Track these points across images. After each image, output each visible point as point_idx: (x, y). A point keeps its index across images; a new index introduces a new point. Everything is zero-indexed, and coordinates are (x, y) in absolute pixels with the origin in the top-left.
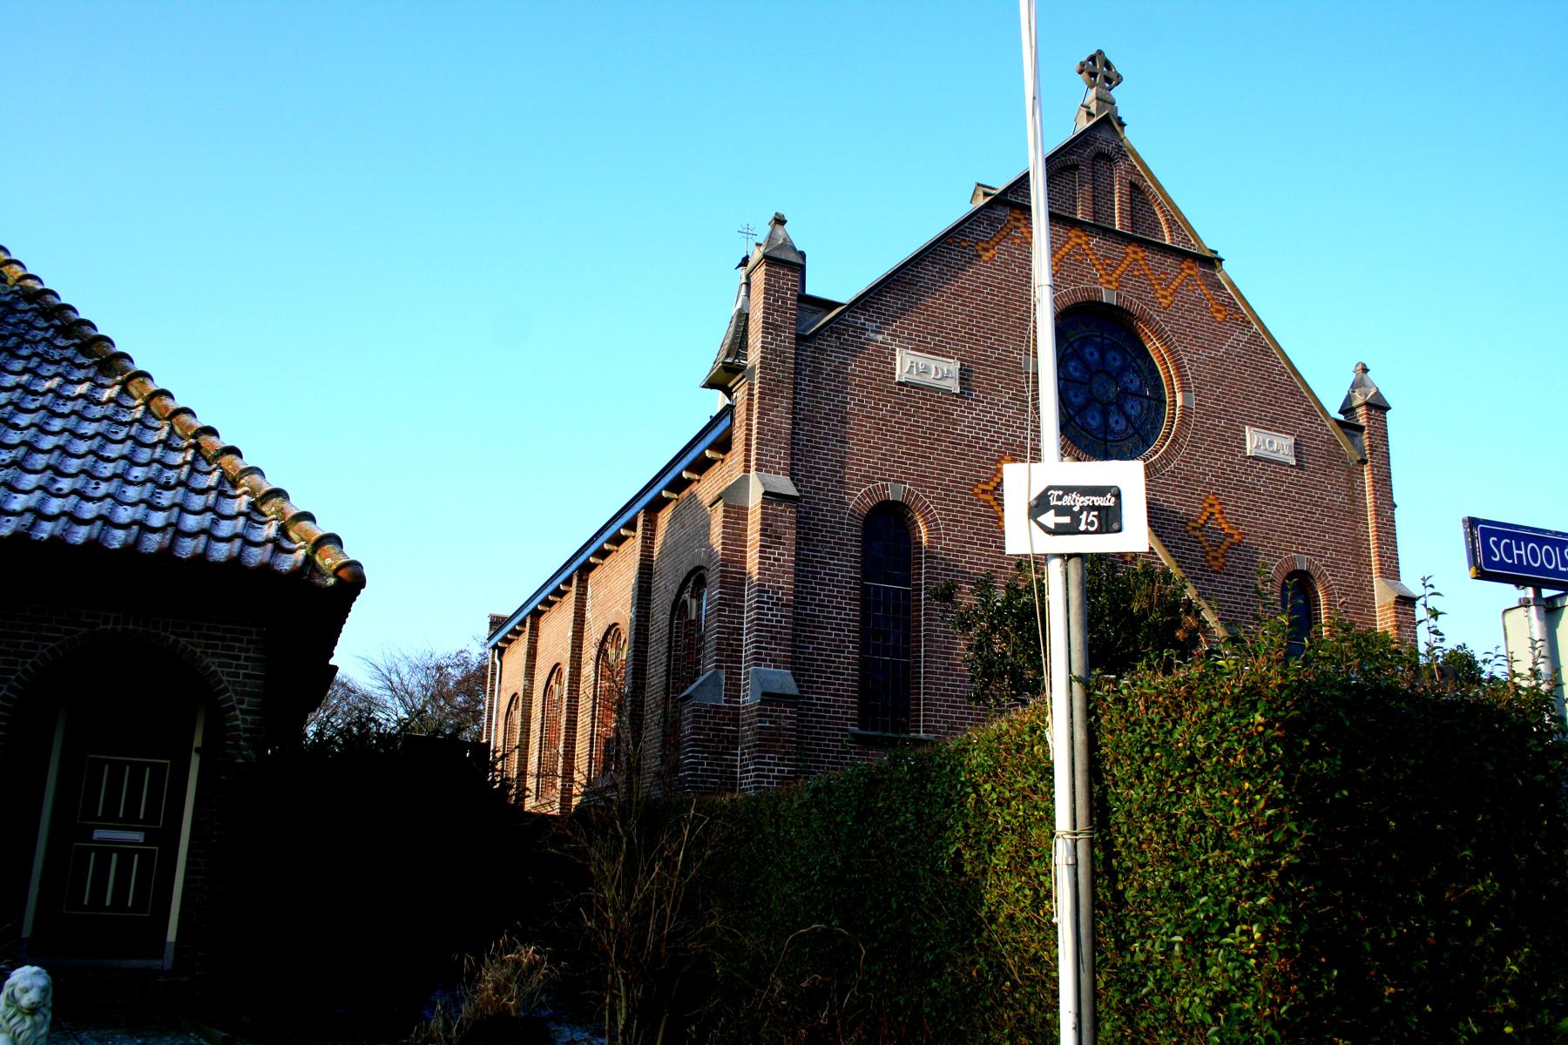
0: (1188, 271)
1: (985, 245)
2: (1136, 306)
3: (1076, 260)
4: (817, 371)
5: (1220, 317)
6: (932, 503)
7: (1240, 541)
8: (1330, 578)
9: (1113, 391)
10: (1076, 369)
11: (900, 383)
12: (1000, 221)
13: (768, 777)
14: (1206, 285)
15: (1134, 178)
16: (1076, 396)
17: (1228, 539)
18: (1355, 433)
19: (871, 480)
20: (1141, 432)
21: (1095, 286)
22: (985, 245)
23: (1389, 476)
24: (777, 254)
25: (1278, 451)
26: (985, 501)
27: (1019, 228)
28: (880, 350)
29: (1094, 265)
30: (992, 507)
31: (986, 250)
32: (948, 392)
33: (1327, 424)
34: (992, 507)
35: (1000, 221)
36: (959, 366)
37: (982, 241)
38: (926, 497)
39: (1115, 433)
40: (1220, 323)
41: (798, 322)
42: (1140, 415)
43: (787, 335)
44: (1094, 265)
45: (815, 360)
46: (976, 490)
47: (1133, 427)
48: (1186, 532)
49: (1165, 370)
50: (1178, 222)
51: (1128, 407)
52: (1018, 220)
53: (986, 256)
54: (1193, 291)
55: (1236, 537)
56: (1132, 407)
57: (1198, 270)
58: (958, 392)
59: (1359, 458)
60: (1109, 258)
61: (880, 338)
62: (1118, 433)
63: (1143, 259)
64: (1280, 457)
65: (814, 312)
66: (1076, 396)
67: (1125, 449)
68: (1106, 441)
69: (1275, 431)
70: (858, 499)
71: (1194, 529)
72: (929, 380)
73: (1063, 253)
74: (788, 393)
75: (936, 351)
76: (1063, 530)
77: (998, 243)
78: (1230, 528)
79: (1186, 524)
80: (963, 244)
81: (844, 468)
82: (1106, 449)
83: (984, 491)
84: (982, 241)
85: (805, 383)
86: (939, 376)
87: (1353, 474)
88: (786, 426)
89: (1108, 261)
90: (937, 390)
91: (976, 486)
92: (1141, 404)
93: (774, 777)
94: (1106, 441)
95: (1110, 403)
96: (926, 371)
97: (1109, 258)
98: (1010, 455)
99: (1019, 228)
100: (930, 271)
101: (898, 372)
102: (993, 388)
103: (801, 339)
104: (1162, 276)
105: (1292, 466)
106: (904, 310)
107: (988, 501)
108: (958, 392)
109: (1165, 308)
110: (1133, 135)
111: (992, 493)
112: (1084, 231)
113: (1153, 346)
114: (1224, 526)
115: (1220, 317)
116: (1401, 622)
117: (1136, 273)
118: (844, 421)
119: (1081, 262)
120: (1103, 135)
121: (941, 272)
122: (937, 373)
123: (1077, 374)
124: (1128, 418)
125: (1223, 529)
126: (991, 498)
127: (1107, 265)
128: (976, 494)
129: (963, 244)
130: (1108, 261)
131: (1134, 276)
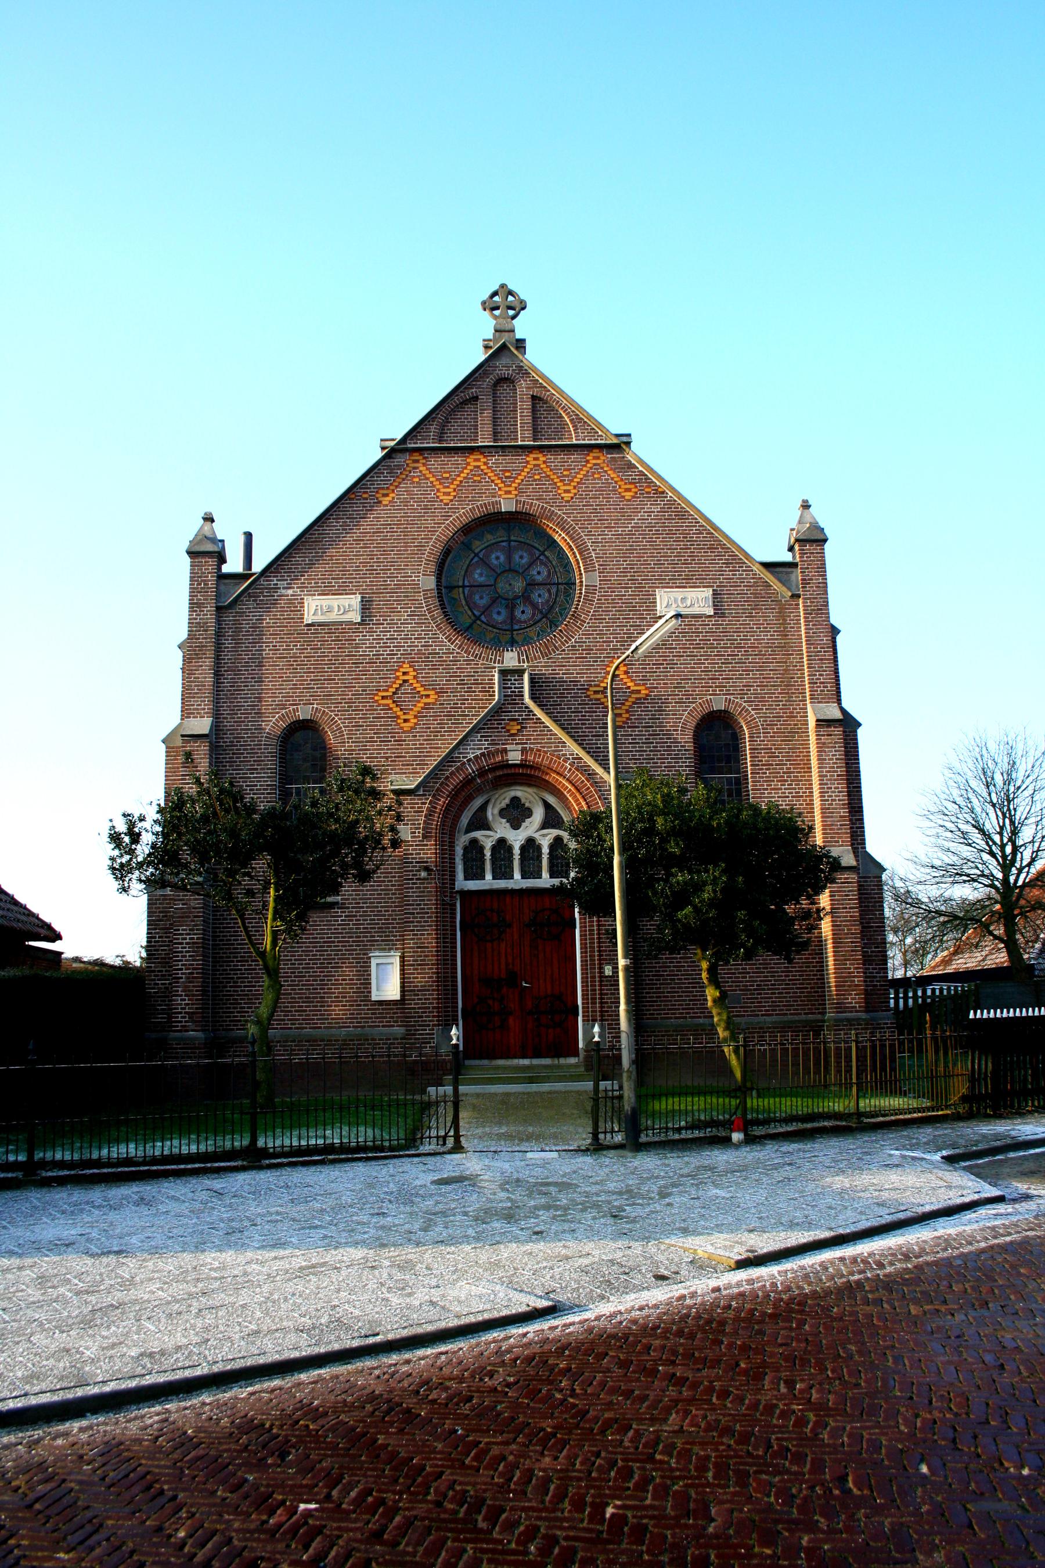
0: (594, 462)
1: (385, 492)
2: (535, 506)
3: (475, 481)
4: (238, 630)
5: (628, 495)
6: (337, 715)
7: (647, 695)
8: (753, 712)
9: (519, 585)
10: (481, 575)
11: (308, 625)
12: (399, 467)
13: (182, 943)
14: (614, 470)
15: (536, 392)
16: (481, 598)
17: (634, 696)
18: (790, 570)
19: (283, 706)
20: (549, 616)
21: (494, 500)
22: (385, 492)
23: (826, 604)
24: (193, 550)
25: (692, 605)
26: (384, 705)
27: (417, 468)
28: (290, 602)
29: (493, 481)
30: (391, 709)
31: (387, 495)
32: (351, 623)
33: (754, 568)
34: (391, 709)
35: (399, 467)
36: (359, 599)
37: (383, 488)
38: (332, 711)
39: (521, 622)
40: (629, 500)
41: (218, 595)
42: (548, 601)
43: (209, 610)
44: (493, 481)
45: (236, 622)
46: (376, 698)
47: (541, 612)
48: (588, 696)
49: (573, 557)
50: (582, 420)
51: (534, 597)
52: (417, 461)
53: (386, 501)
54: (599, 479)
55: (643, 692)
56: (540, 596)
57: (605, 457)
58: (359, 620)
59: (790, 594)
60: (509, 471)
61: (290, 592)
62: (525, 622)
63: (544, 462)
64: (696, 610)
65: (236, 584)
66: (481, 598)
67: (532, 634)
68: (512, 630)
69: (691, 587)
70: (273, 723)
71: (596, 692)
72: (333, 617)
73: (459, 479)
74: (210, 654)
75: (342, 591)
76: (827, 665)
77: (397, 487)
78: (636, 685)
79: (587, 689)
80: (365, 496)
81: (260, 701)
82: (512, 637)
83: (383, 698)
84: (383, 488)
85: (228, 643)
86: (342, 611)
87: (783, 611)
88: (210, 679)
89: (507, 474)
90: (341, 623)
91: (377, 695)
92: (549, 591)
93: (187, 943)
94: (512, 630)
95: (517, 597)
96: (330, 610)
97: (509, 471)
98: (409, 662)
99: (417, 468)
100: (335, 525)
101: (306, 616)
102: (393, 610)
103: (219, 609)
104: (565, 473)
105: (710, 616)
106: (311, 564)
107: (388, 705)
108: (359, 620)
109: (568, 502)
110: (535, 356)
111: (391, 697)
112: (482, 453)
113: (560, 537)
114: (629, 684)
115: (628, 495)
116: (824, 743)
117: (537, 477)
118: (260, 665)
119: (480, 482)
120: (503, 360)
121: (345, 524)
122: (339, 610)
123: (482, 579)
124: (534, 606)
125: (629, 688)
126: (390, 702)
127: (506, 477)
128: (377, 701)
129: (365, 496)
130: (507, 474)
131: (535, 480)
